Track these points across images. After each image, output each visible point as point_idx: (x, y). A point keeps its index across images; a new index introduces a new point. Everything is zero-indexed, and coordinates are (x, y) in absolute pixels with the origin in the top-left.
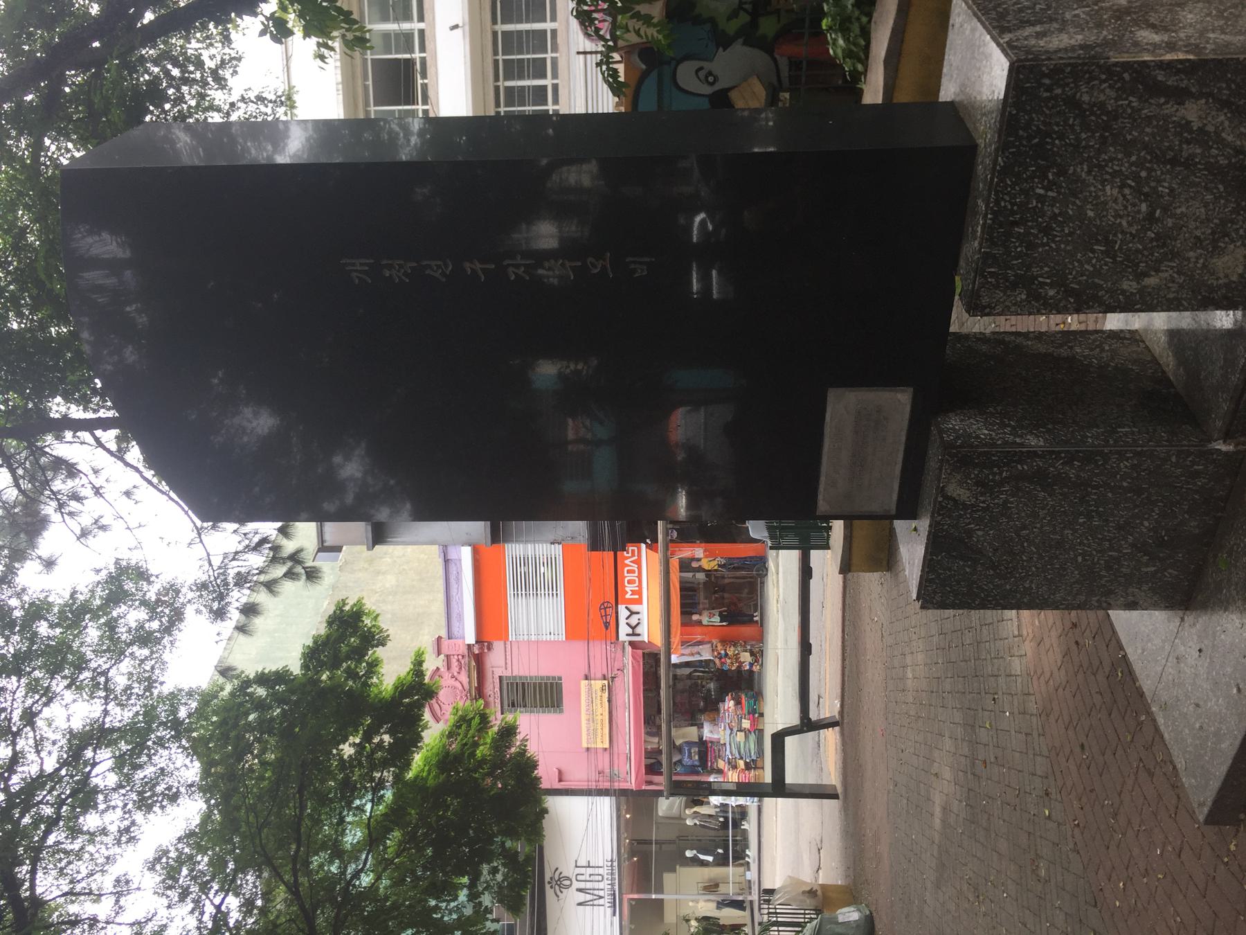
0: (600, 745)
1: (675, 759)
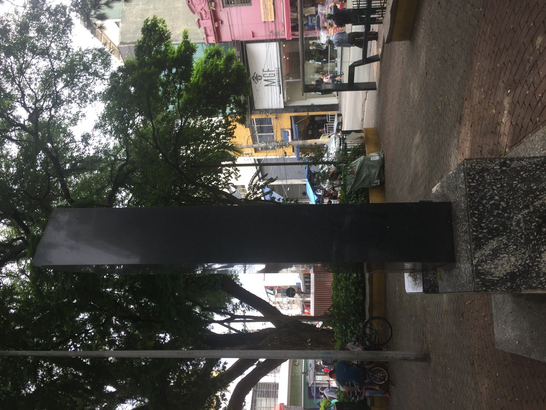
0: (270, 20)
1: (305, 23)
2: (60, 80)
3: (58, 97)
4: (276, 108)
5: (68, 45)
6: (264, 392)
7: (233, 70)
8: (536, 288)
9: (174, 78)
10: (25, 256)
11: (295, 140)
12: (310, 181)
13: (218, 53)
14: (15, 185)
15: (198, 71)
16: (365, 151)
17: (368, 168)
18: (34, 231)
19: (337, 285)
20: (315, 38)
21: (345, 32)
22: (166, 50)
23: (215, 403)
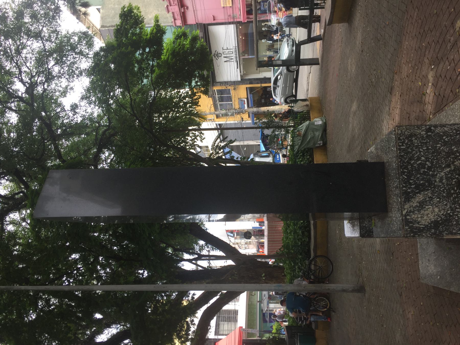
0: (228, 5)
1: (258, 8)
2: (51, 59)
3: (50, 73)
4: (234, 80)
5: (58, 29)
6: (225, 318)
7: (197, 49)
8: (455, 234)
9: (147, 56)
10: (25, 207)
11: (250, 108)
12: (263, 142)
13: (184, 35)
14: (16, 148)
15: (168, 50)
16: (310, 116)
17: (313, 131)
18: (33, 186)
19: (286, 229)
20: (267, 21)
21: (292, 16)
22: (141, 32)
23: (186, 327)
